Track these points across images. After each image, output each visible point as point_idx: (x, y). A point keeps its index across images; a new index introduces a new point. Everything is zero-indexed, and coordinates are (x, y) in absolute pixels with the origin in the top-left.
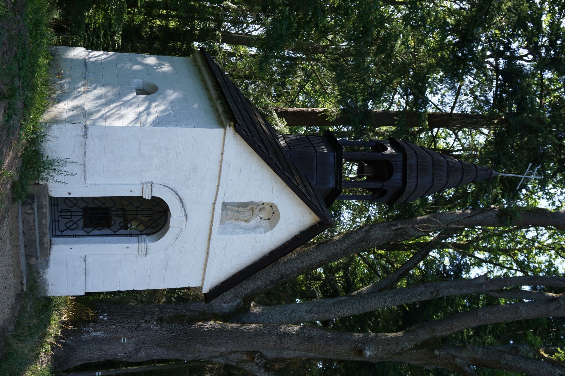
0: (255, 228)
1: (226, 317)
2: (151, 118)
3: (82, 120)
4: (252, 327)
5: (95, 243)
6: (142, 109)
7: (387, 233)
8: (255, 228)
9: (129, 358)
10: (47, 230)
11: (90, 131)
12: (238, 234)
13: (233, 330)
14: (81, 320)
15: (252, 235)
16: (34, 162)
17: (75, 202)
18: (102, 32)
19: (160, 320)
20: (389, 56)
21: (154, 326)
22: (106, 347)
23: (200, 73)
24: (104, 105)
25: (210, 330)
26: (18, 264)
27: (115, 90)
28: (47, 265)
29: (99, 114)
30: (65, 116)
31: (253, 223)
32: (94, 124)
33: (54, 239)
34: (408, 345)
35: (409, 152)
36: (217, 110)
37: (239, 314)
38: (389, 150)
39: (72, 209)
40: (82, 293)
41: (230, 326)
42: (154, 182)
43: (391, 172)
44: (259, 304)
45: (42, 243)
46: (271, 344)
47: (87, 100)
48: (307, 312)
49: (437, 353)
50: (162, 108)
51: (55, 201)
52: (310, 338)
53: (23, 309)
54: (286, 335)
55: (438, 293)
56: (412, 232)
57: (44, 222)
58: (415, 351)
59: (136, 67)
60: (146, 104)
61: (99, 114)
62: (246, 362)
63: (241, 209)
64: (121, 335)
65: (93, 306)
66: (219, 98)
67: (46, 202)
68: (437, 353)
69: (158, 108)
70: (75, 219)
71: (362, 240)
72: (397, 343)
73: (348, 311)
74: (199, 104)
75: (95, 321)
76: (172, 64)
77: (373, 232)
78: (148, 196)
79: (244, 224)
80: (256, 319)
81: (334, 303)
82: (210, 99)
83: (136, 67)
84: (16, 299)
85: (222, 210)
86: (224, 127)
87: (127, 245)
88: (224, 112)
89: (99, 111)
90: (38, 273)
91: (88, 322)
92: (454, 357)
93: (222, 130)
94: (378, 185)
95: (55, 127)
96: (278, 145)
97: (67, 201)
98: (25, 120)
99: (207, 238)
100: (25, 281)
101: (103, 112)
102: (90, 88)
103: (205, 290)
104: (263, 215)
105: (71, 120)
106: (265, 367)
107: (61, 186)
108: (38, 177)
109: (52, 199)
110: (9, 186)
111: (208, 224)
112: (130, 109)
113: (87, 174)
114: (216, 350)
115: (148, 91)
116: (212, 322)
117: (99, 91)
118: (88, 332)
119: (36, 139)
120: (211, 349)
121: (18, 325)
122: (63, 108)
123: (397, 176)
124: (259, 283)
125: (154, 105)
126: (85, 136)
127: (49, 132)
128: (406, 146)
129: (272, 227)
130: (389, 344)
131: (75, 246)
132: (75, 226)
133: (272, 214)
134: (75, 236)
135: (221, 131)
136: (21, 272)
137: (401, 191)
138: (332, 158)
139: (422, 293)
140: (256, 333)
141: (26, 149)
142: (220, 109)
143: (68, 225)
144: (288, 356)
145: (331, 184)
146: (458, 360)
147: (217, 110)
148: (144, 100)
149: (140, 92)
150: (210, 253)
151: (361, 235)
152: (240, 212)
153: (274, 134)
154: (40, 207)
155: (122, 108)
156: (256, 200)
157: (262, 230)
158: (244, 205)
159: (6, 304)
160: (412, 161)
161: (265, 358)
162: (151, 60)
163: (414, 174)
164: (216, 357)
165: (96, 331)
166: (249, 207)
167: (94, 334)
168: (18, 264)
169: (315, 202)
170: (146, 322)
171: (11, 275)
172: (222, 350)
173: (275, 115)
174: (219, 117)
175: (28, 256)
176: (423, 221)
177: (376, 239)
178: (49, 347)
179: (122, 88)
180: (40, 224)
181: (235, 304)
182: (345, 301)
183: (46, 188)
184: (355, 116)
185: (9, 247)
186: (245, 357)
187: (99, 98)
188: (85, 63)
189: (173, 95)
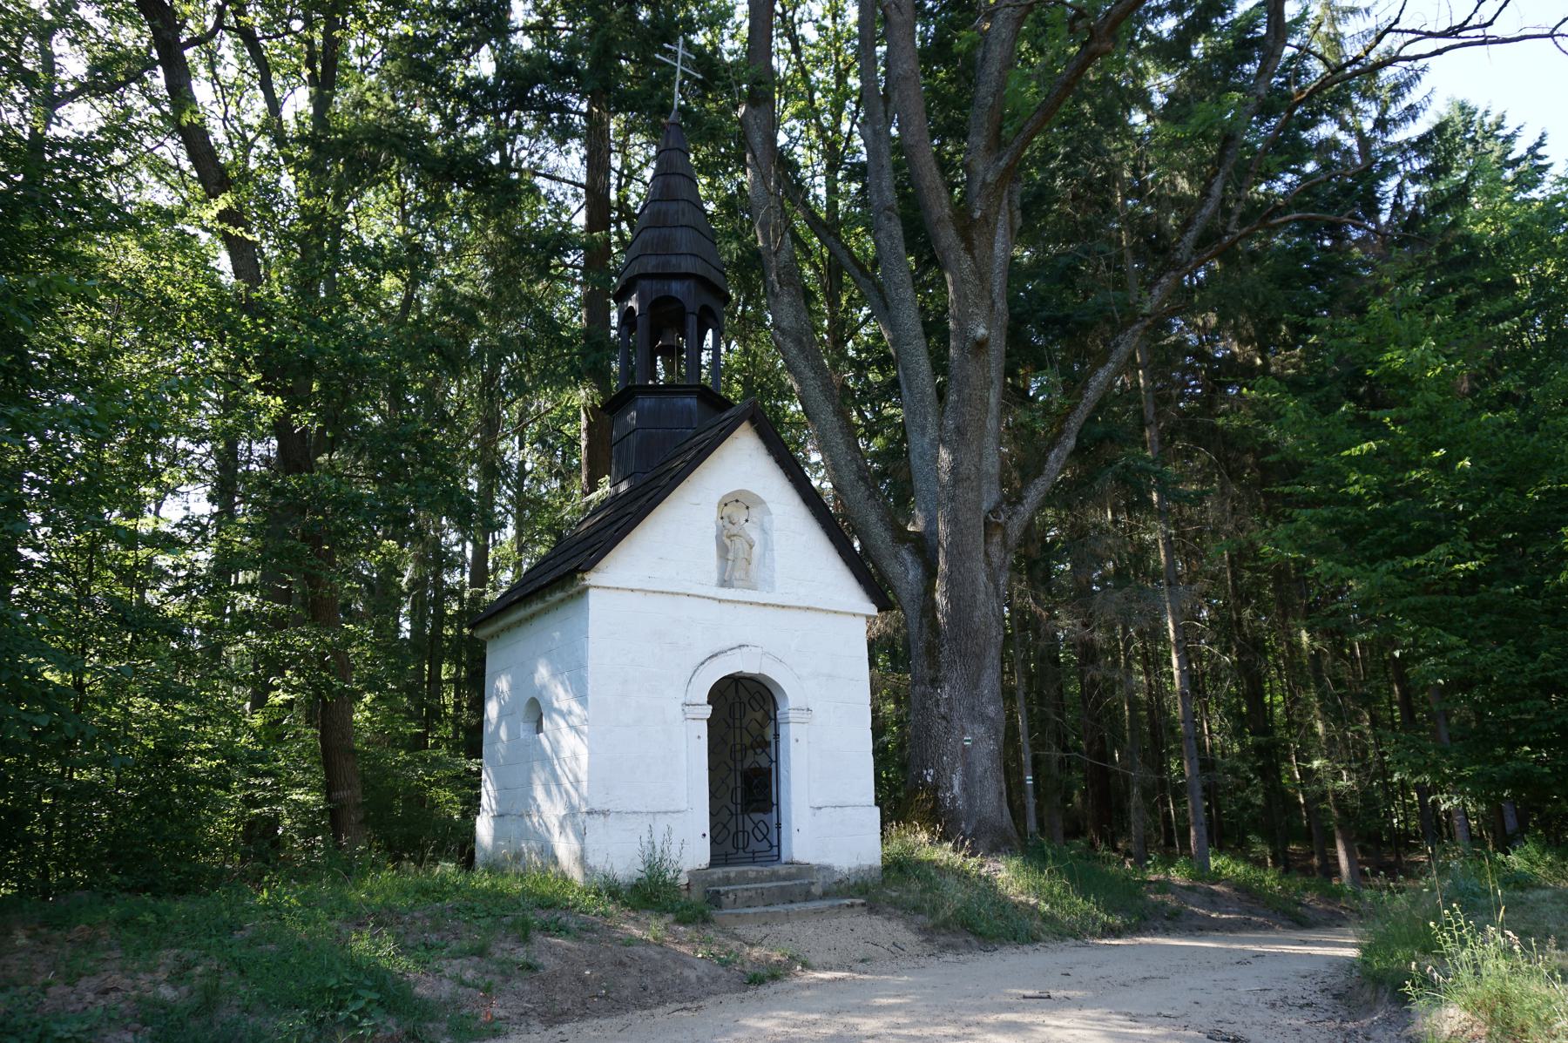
0: (764, 531)
1: (930, 572)
2: (576, 708)
3: (580, 818)
4: (942, 529)
5: (789, 792)
6: (562, 723)
7: (786, 299)
8: (764, 531)
9: (997, 731)
10: (767, 870)
11: (597, 806)
12: (773, 560)
13: (949, 562)
14: (934, 810)
15: (775, 536)
16: (650, 893)
17: (720, 826)
18: (467, 790)
19: (935, 682)
20: (481, 303)
21: (945, 692)
22: (979, 770)
23: (508, 628)
24: (559, 784)
25: (950, 600)
26: (816, 912)
27: (537, 766)
28: (828, 868)
29: (572, 791)
30: (576, 846)
31: (755, 535)
32: (586, 801)
33: (784, 858)
34: (966, 264)
35: (636, 269)
36: (562, 601)
37: (923, 548)
38: (633, 303)
39: (733, 830)
40: (878, 809)
41: (942, 566)
42: (682, 700)
43: (670, 299)
44: (910, 518)
45: (788, 877)
46: (971, 495)
47: (550, 811)
48: (924, 435)
49: (977, 214)
50: (560, 691)
51: (719, 857)
52: (960, 431)
53: (894, 903)
54: (954, 470)
55: (890, 209)
56: (784, 256)
57: (752, 875)
58: (976, 252)
59: (503, 734)
60: (555, 716)
61: (572, 791)
62: (1005, 536)
63: (731, 556)
64: (959, 747)
65: (902, 788)
66: (542, 598)
67: (719, 872)
68: (977, 214)
69: (561, 697)
70: (749, 826)
71: (798, 342)
72: (963, 281)
73: (923, 365)
74: (551, 631)
75: (935, 788)
76: (497, 675)
77: (784, 324)
78: (708, 711)
79: (757, 550)
80: (931, 521)
81: (909, 388)
82: (546, 611)
83: (503, 734)
84: (877, 913)
85: (731, 586)
86: (587, 588)
87: (792, 741)
88: (562, 589)
89: (567, 792)
90: (841, 881)
91: (936, 799)
92: (984, 184)
93: (591, 591)
94: (692, 321)
95: (591, 862)
96: (627, 494)
97: (719, 840)
98: (575, 906)
99: (781, 611)
100: (848, 902)
101: (568, 786)
102: (534, 808)
103: (872, 610)
104: (740, 516)
105: (581, 835)
106: (1015, 504)
107: (690, 848)
108: (672, 886)
109: (714, 863)
110: (681, 928)
111: (755, 610)
112: (563, 743)
113: (672, 808)
114: (982, 588)
115: (536, 712)
116: (937, 596)
117: (539, 793)
118: (954, 800)
119: (612, 890)
120: (981, 597)
121: (918, 909)
122: (565, 849)
123: (677, 288)
124: (873, 518)
125: (556, 705)
126: (605, 813)
127: (600, 869)
128: (626, 276)
129: (762, 502)
130: (966, 296)
131: (795, 824)
132: (761, 825)
133: (738, 502)
134: (779, 826)
135: (596, 601)
136: (832, 907)
137: (704, 283)
138: (647, 402)
139: (890, 237)
140: (953, 521)
141: (625, 904)
142: (559, 595)
143: (760, 837)
144: (997, 466)
145: (692, 402)
146: (990, 178)
147: (562, 601)
148: (551, 719)
149: (539, 728)
150: (806, 605)
151: (789, 345)
152: (733, 553)
153: (615, 499)
154: (727, 881)
155: (562, 755)
156: (713, 532)
157: (766, 519)
158: (723, 550)
159: (880, 928)
160: (650, 264)
161: (999, 504)
162: (492, 709)
163: (674, 260)
164: (997, 587)
165: (952, 786)
166: (728, 542)
167: (956, 790)
168: (816, 912)
169: (716, 430)
170: (938, 706)
171: (835, 922)
172: (982, 578)
173: (593, 496)
174: (572, 596)
175: (808, 896)
176: (766, 237)
177: (797, 319)
178: (973, 861)
179: (533, 757)
180: (755, 880)
181: (908, 558)
182: (905, 369)
183: (694, 874)
184: (589, 359)
185: (787, 927)
186: (997, 539)
187: (548, 793)
188: (499, 817)
189: (543, 673)
